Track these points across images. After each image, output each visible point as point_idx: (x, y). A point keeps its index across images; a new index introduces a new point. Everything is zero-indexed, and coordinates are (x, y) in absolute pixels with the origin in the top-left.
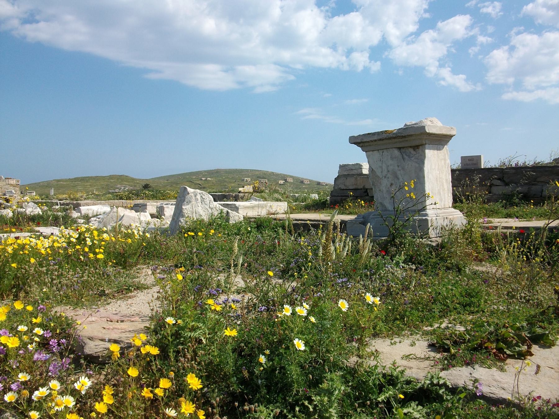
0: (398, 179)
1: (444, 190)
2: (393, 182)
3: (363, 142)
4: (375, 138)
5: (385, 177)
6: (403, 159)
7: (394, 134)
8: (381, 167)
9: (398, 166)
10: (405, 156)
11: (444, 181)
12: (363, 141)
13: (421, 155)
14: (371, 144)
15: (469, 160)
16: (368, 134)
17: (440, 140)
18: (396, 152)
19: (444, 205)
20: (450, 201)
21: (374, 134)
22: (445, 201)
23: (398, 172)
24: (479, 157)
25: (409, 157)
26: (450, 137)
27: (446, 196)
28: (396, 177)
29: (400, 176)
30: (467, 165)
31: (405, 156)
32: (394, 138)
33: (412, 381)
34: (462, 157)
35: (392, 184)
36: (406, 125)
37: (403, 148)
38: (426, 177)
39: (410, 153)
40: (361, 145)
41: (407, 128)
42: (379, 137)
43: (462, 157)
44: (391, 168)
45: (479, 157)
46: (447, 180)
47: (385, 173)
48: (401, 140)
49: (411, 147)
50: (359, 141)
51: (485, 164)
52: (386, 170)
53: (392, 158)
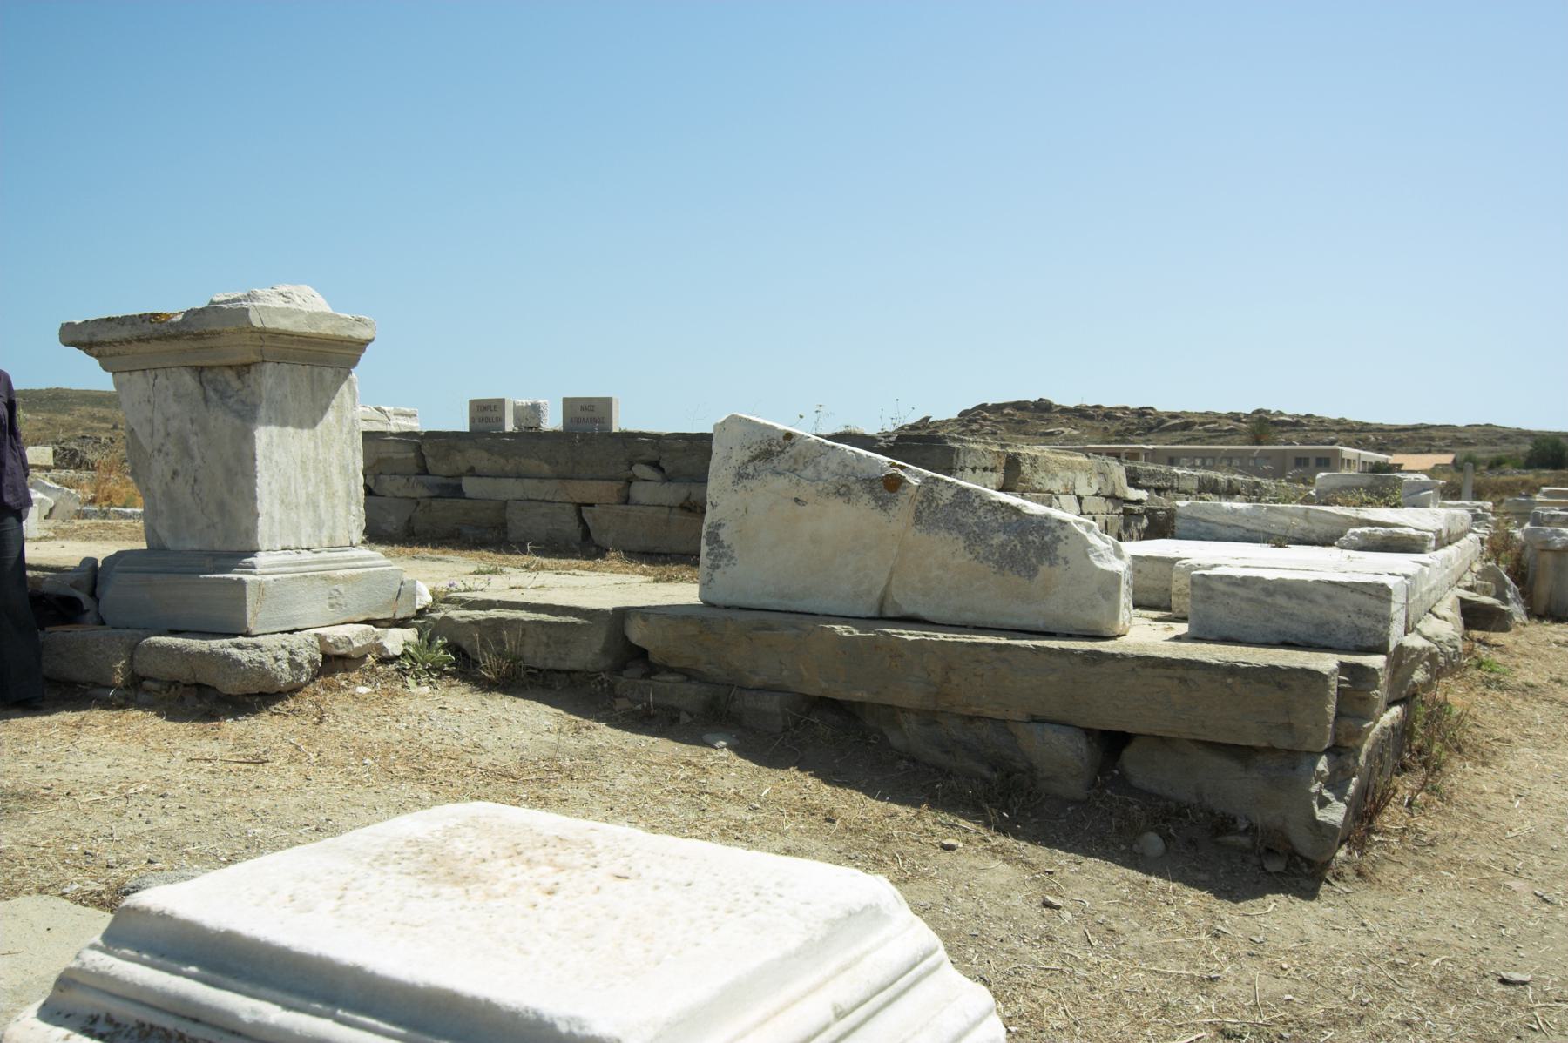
0: (192, 458)
1: (332, 495)
2: (179, 467)
3: (82, 337)
4: (125, 333)
5: (160, 451)
6: (206, 400)
7: (172, 325)
8: (150, 421)
9: (192, 422)
10: (211, 393)
11: (335, 470)
12: (95, 339)
13: (253, 393)
14: (121, 349)
15: (582, 409)
16: (109, 320)
17: (328, 357)
18: (188, 381)
19: (331, 538)
20: (353, 527)
21: (122, 321)
22: (334, 529)
23: (193, 439)
24: (607, 403)
25: (223, 396)
26: (362, 344)
27: (341, 511)
28: (186, 452)
29: (196, 452)
30: (579, 420)
31: (211, 393)
32: (176, 337)
33: (1194, 423)
34: (565, 400)
35: (175, 473)
36: (212, 302)
37: (211, 368)
38: (259, 457)
39: (228, 383)
40: (95, 350)
41: (214, 309)
42: (136, 332)
43: (565, 400)
44: (175, 425)
45: (607, 403)
46: (344, 468)
47: (159, 439)
48: (195, 345)
49: (230, 367)
50: (84, 338)
51: (622, 421)
52: (162, 433)
53: (178, 397)
